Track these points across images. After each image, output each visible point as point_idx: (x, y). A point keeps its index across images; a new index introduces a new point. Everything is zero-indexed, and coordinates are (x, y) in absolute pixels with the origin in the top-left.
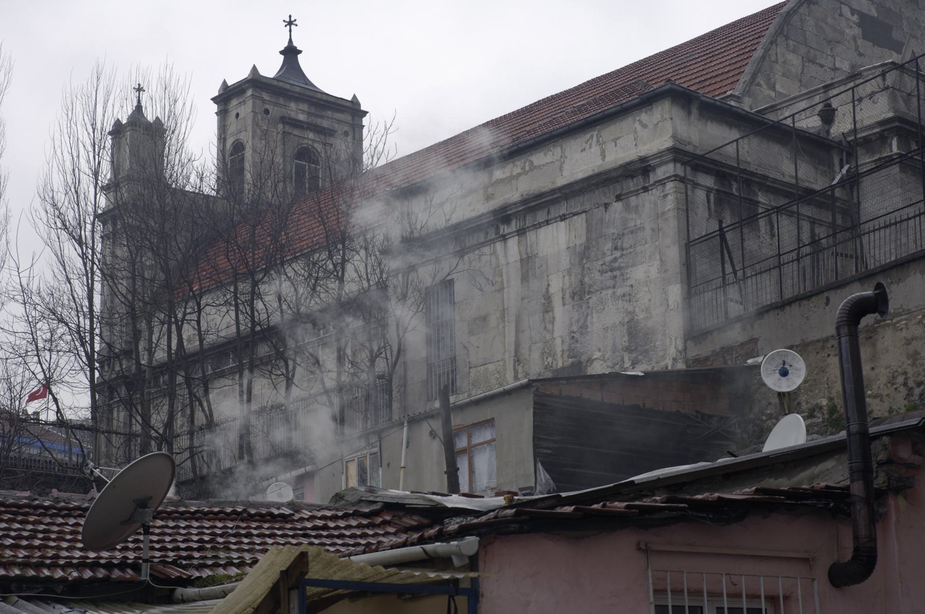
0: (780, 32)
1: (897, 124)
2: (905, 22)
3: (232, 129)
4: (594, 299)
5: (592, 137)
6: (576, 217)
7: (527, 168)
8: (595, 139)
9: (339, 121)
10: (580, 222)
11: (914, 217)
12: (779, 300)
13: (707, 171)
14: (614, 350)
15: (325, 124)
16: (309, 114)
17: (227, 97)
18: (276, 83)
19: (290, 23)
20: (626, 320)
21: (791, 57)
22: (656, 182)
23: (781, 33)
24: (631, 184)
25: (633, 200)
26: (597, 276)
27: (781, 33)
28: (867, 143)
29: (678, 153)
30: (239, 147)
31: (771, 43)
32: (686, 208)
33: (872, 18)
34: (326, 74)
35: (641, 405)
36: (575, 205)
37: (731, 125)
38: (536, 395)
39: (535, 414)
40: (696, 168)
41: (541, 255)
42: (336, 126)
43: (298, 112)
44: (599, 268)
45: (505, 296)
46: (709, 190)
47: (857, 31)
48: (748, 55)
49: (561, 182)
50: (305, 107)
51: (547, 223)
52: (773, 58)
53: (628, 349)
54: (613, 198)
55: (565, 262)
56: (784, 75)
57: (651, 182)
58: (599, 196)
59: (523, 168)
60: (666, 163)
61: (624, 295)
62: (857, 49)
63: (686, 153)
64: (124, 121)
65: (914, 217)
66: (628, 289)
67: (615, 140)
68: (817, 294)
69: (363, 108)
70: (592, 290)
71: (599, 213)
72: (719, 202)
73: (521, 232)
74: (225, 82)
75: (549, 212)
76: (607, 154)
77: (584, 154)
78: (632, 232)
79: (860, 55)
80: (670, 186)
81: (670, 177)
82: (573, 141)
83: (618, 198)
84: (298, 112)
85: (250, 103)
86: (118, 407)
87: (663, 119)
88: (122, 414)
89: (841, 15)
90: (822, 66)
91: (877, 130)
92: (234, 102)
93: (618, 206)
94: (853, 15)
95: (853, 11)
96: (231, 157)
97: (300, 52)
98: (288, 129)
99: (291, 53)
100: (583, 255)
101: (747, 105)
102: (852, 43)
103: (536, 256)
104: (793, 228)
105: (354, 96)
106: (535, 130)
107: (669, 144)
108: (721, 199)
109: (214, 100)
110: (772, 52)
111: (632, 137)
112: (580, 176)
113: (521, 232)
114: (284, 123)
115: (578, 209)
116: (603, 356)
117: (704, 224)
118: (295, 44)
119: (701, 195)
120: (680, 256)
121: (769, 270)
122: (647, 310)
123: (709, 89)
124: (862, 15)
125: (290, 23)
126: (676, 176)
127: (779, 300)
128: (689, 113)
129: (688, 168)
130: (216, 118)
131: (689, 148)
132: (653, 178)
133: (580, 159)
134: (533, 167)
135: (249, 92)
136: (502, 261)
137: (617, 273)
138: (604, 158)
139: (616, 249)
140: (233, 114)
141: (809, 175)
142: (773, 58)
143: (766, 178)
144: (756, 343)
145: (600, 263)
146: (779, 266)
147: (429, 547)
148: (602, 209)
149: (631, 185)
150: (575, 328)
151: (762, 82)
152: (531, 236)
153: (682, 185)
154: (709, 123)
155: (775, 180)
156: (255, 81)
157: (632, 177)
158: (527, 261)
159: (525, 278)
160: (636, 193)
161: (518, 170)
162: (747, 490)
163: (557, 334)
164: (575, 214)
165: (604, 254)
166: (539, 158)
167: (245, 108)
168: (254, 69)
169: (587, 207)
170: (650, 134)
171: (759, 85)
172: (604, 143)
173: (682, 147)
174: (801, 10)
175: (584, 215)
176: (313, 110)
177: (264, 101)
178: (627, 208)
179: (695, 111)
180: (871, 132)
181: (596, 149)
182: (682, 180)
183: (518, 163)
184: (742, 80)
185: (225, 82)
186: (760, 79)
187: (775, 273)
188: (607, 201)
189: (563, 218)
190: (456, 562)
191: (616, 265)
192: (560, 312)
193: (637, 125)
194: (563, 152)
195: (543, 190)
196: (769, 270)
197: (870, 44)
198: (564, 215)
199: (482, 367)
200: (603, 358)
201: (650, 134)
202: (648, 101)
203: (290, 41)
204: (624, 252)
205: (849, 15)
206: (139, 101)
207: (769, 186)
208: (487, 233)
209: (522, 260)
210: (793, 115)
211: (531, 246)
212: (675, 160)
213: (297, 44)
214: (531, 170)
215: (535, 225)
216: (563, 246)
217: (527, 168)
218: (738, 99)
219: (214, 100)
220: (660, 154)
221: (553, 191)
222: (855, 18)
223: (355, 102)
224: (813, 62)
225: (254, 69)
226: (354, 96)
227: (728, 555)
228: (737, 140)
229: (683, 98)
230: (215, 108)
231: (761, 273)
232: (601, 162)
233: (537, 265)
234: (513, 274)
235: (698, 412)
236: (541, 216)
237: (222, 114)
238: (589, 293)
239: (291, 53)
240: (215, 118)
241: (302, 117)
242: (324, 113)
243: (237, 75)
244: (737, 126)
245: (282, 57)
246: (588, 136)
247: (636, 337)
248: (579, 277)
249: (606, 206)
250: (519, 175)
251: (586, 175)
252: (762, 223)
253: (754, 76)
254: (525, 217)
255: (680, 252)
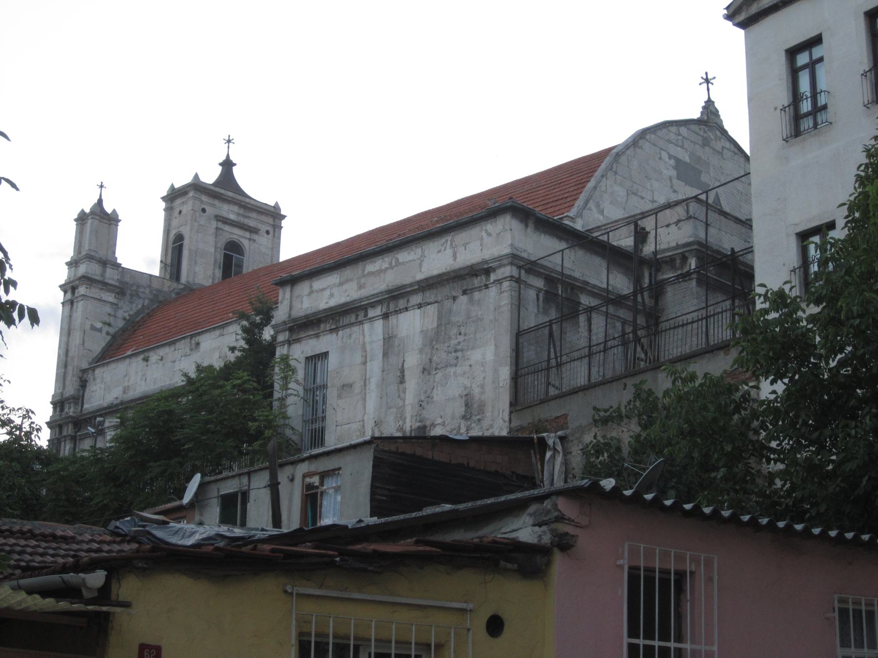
0: (610, 168)
1: (695, 247)
2: (711, 169)
3: (175, 223)
4: (439, 376)
5: (447, 241)
6: (429, 306)
7: (394, 264)
8: (449, 242)
9: (262, 222)
10: (432, 310)
11: (697, 321)
12: (586, 383)
13: (538, 274)
14: (453, 418)
15: (252, 223)
16: (238, 214)
17: (174, 196)
18: (213, 188)
19: (229, 141)
20: (465, 393)
21: (617, 188)
22: (495, 281)
23: (611, 169)
24: (476, 282)
25: (477, 295)
26: (444, 356)
27: (611, 169)
28: (670, 262)
29: (514, 258)
30: (180, 238)
31: (602, 176)
32: (518, 304)
33: (686, 163)
34: (254, 184)
35: (466, 463)
36: (430, 296)
37: (561, 239)
38: (375, 450)
39: (374, 466)
40: (529, 271)
41: (399, 336)
42: (260, 226)
43: (230, 212)
44: (445, 349)
45: (368, 368)
46: (539, 290)
47: (673, 173)
48: (580, 186)
49: (420, 277)
50: (236, 209)
51: (406, 309)
52: (603, 189)
53: (464, 417)
54: (460, 291)
55: (418, 342)
56: (611, 203)
57: (492, 281)
58: (446, 291)
59: (390, 264)
60: (504, 266)
61: (464, 373)
62: (672, 187)
63: (522, 259)
64: (87, 211)
65: (697, 321)
66: (467, 368)
67: (465, 246)
68: (617, 380)
69: (282, 213)
70: (439, 367)
71: (448, 303)
72: (547, 300)
73: (386, 316)
74: (172, 185)
75: (408, 301)
76: (458, 255)
77: (440, 254)
78: (473, 322)
79: (675, 191)
80: (506, 284)
81: (506, 278)
82: (431, 244)
83: (465, 292)
84: (230, 212)
85: (190, 203)
86: (65, 441)
87: (505, 230)
88: (68, 447)
89: (660, 159)
90: (642, 198)
91: (680, 251)
92: (179, 201)
93: (464, 299)
94: (670, 159)
95: (670, 157)
96: (175, 248)
97: (235, 165)
98: (220, 225)
99: (228, 165)
100: (434, 339)
101: (579, 226)
102: (668, 182)
103: (396, 336)
104: (603, 323)
105: (277, 203)
106: (404, 234)
107: (507, 251)
108: (549, 297)
109: (163, 198)
110: (603, 184)
111: (478, 243)
112: (435, 272)
113: (386, 316)
114: (218, 220)
115: (432, 300)
116: (444, 422)
117: (532, 318)
118: (231, 158)
119: (532, 294)
120: (511, 344)
121: (581, 358)
122: (482, 386)
123: (552, 210)
124: (678, 161)
125: (229, 141)
126: (512, 277)
127: (586, 383)
128: (527, 226)
129: (523, 272)
130: (163, 213)
131: (524, 255)
132: (493, 277)
133: (437, 259)
134: (398, 263)
135: (191, 194)
136: (367, 339)
137: (459, 354)
138: (455, 258)
139: (460, 334)
140: (177, 211)
141: (621, 284)
142: (603, 189)
143: (587, 283)
144: (566, 418)
145: (447, 345)
146: (590, 355)
147: (66, 576)
148: (451, 300)
149: (477, 282)
150: (423, 398)
151: (593, 208)
152: (393, 319)
153: (514, 284)
154: (543, 235)
155: (595, 286)
156: (196, 186)
157: (477, 276)
158: (389, 340)
159: (385, 354)
160: (479, 289)
161: (385, 265)
162: (409, 540)
163: (407, 402)
164: (429, 304)
165: (450, 338)
166: (404, 256)
167: (187, 206)
168: (196, 176)
169: (440, 299)
170: (496, 240)
171: (590, 209)
172: (456, 246)
173: (519, 253)
174: (628, 152)
175: (436, 304)
176: (242, 211)
177: (202, 202)
178: (471, 301)
179: (531, 224)
180: (675, 252)
181: (449, 252)
182: (518, 281)
183: (387, 259)
184: (576, 205)
185: (172, 185)
186: (591, 204)
187: (586, 360)
188: (454, 294)
189: (420, 306)
190: (86, 594)
191: (459, 347)
192: (412, 384)
193: (483, 233)
194: (423, 252)
195: (404, 283)
196: (581, 358)
197: (683, 184)
198: (420, 304)
199: (347, 426)
200: (443, 424)
201: (496, 240)
202: (492, 214)
203: (228, 156)
204: (467, 338)
205: (667, 160)
206: (101, 195)
207: (589, 291)
208: (357, 316)
209: (384, 339)
210: (608, 233)
211: (392, 328)
212: (512, 264)
213: (233, 158)
214: (396, 266)
215: (396, 311)
216: (418, 330)
217: (394, 264)
218: (572, 219)
219: (163, 198)
220: (499, 258)
221: (411, 285)
222: (672, 162)
223: (277, 207)
224: (635, 194)
225: (196, 176)
226: (277, 203)
227: (380, 602)
228: (562, 251)
229: (523, 214)
230: (163, 205)
231: (574, 360)
232: (453, 262)
233: (396, 344)
234: (376, 347)
235: (513, 472)
236: (402, 303)
237: (169, 210)
238: (436, 369)
239: (228, 165)
240: (162, 214)
241: (232, 217)
242: (251, 215)
243: (182, 180)
244: (567, 240)
245: (220, 168)
246: (444, 240)
247: (471, 408)
248: (429, 355)
249: (454, 298)
250: (387, 269)
251: (440, 272)
252: (582, 318)
253: (587, 203)
254: (389, 304)
255: (511, 340)
